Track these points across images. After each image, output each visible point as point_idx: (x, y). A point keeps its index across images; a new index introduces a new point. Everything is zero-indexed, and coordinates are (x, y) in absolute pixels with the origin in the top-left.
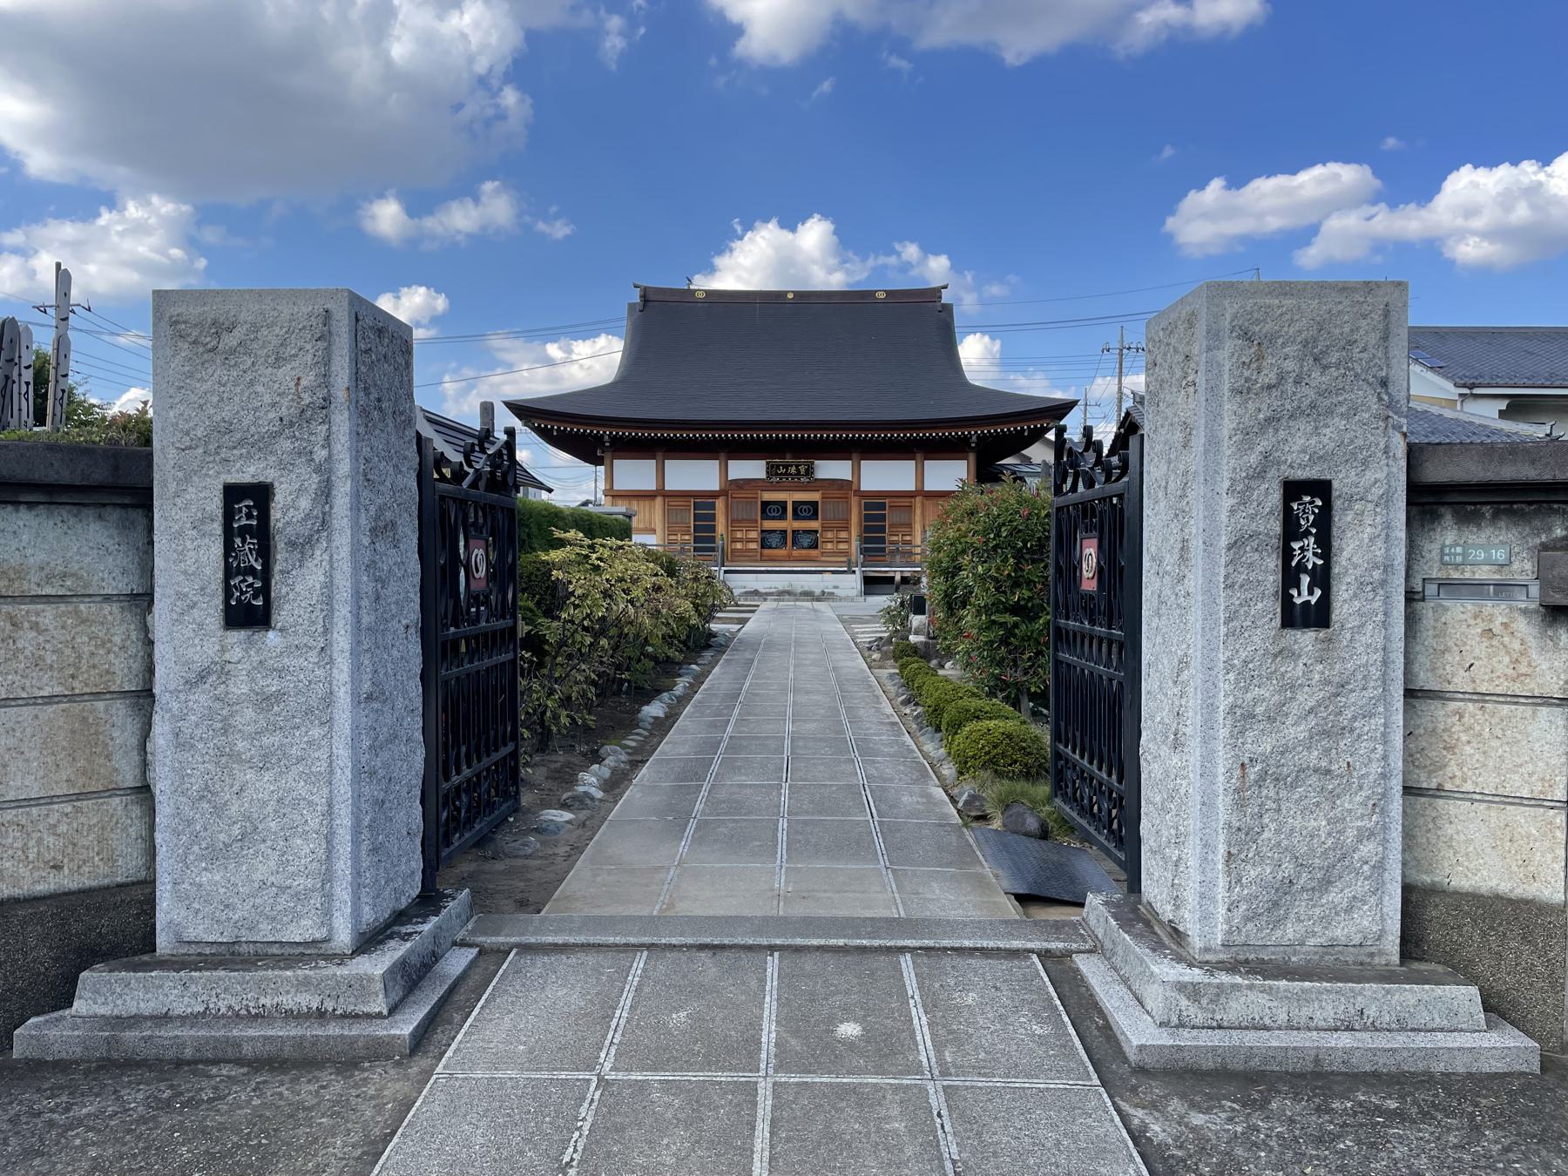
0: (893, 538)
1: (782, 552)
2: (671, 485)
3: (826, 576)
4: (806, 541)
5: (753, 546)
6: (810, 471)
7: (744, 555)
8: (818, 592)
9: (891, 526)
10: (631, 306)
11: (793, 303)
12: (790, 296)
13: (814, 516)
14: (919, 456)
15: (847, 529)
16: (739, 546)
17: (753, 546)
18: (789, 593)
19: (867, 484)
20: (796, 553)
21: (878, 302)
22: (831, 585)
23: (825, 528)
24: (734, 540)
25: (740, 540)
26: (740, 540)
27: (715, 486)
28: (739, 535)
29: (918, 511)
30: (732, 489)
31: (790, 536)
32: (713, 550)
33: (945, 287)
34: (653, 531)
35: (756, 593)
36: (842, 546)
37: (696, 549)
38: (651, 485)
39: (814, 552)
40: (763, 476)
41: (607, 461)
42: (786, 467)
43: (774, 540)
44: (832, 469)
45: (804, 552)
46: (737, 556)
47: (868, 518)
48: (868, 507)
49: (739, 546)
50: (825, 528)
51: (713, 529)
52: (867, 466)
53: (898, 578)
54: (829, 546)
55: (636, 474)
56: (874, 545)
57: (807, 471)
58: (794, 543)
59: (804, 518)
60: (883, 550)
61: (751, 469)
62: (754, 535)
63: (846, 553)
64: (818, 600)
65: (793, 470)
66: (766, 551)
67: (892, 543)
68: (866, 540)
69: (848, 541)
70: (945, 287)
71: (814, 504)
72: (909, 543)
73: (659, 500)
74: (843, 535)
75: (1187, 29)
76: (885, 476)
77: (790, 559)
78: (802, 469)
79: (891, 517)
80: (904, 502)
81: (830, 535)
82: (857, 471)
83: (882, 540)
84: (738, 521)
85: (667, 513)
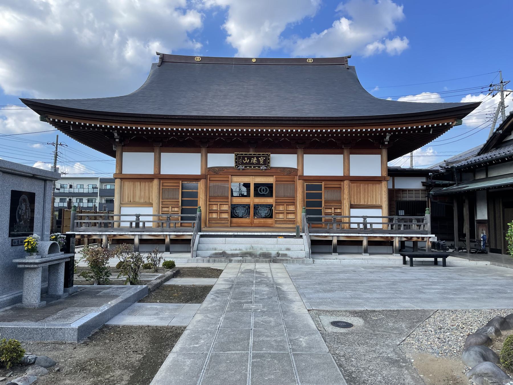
0: (327, 211)
1: (246, 220)
2: (166, 170)
3: (281, 239)
4: (264, 212)
5: (225, 216)
6: (267, 162)
7: (219, 223)
8: (274, 253)
9: (326, 202)
10: (154, 65)
11: (255, 64)
12: (254, 61)
13: (271, 195)
14: (346, 152)
15: (294, 203)
16: (214, 216)
17: (225, 216)
18: (251, 254)
19: (308, 172)
20: (257, 221)
21: (309, 64)
22: (283, 247)
23: (278, 203)
24: (211, 212)
25: (216, 212)
26: (216, 212)
27: (197, 171)
28: (215, 208)
29: (346, 191)
30: (211, 174)
31: (255, 213)
32: (194, 219)
33: (349, 57)
34: (150, 205)
35: (223, 254)
36: (291, 216)
37: (182, 218)
38: (150, 171)
39: (269, 221)
40: (232, 164)
41: (118, 154)
42: (250, 158)
43: (240, 211)
44: (282, 160)
45: (262, 220)
46: (211, 223)
47: (308, 196)
48: (308, 188)
49: (214, 216)
50: (278, 203)
51: (196, 203)
52: (308, 158)
53: (335, 241)
54: (281, 216)
55: (138, 163)
56: (314, 216)
57: (265, 161)
58: (255, 214)
59: (263, 196)
60: (320, 219)
61: (225, 160)
62: (225, 208)
63: (293, 222)
64: (275, 261)
65: (254, 160)
66: (235, 220)
67: (327, 214)
68: (308, 212)
69: (294, 213)
70: (349, 57)
71: (270, 186)
72: (340, 214)
73: (156, 182)
74: (291, 208)
75: (384, 51)
76: (321, 165)
77: (252, 225)
78: (261, 160)
79: (325, 195)
80: (335, 184)
81: (281, 208)
82: (300, 162)
83: (320, 212)
84: (215, 197)
85: (162, 192)
